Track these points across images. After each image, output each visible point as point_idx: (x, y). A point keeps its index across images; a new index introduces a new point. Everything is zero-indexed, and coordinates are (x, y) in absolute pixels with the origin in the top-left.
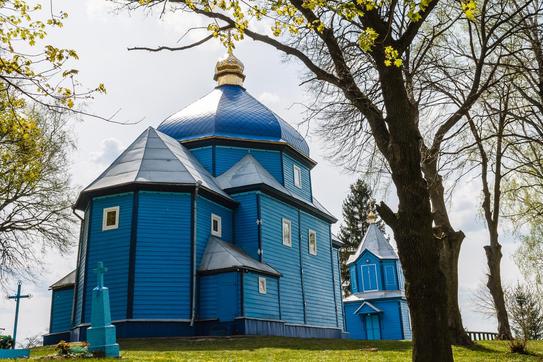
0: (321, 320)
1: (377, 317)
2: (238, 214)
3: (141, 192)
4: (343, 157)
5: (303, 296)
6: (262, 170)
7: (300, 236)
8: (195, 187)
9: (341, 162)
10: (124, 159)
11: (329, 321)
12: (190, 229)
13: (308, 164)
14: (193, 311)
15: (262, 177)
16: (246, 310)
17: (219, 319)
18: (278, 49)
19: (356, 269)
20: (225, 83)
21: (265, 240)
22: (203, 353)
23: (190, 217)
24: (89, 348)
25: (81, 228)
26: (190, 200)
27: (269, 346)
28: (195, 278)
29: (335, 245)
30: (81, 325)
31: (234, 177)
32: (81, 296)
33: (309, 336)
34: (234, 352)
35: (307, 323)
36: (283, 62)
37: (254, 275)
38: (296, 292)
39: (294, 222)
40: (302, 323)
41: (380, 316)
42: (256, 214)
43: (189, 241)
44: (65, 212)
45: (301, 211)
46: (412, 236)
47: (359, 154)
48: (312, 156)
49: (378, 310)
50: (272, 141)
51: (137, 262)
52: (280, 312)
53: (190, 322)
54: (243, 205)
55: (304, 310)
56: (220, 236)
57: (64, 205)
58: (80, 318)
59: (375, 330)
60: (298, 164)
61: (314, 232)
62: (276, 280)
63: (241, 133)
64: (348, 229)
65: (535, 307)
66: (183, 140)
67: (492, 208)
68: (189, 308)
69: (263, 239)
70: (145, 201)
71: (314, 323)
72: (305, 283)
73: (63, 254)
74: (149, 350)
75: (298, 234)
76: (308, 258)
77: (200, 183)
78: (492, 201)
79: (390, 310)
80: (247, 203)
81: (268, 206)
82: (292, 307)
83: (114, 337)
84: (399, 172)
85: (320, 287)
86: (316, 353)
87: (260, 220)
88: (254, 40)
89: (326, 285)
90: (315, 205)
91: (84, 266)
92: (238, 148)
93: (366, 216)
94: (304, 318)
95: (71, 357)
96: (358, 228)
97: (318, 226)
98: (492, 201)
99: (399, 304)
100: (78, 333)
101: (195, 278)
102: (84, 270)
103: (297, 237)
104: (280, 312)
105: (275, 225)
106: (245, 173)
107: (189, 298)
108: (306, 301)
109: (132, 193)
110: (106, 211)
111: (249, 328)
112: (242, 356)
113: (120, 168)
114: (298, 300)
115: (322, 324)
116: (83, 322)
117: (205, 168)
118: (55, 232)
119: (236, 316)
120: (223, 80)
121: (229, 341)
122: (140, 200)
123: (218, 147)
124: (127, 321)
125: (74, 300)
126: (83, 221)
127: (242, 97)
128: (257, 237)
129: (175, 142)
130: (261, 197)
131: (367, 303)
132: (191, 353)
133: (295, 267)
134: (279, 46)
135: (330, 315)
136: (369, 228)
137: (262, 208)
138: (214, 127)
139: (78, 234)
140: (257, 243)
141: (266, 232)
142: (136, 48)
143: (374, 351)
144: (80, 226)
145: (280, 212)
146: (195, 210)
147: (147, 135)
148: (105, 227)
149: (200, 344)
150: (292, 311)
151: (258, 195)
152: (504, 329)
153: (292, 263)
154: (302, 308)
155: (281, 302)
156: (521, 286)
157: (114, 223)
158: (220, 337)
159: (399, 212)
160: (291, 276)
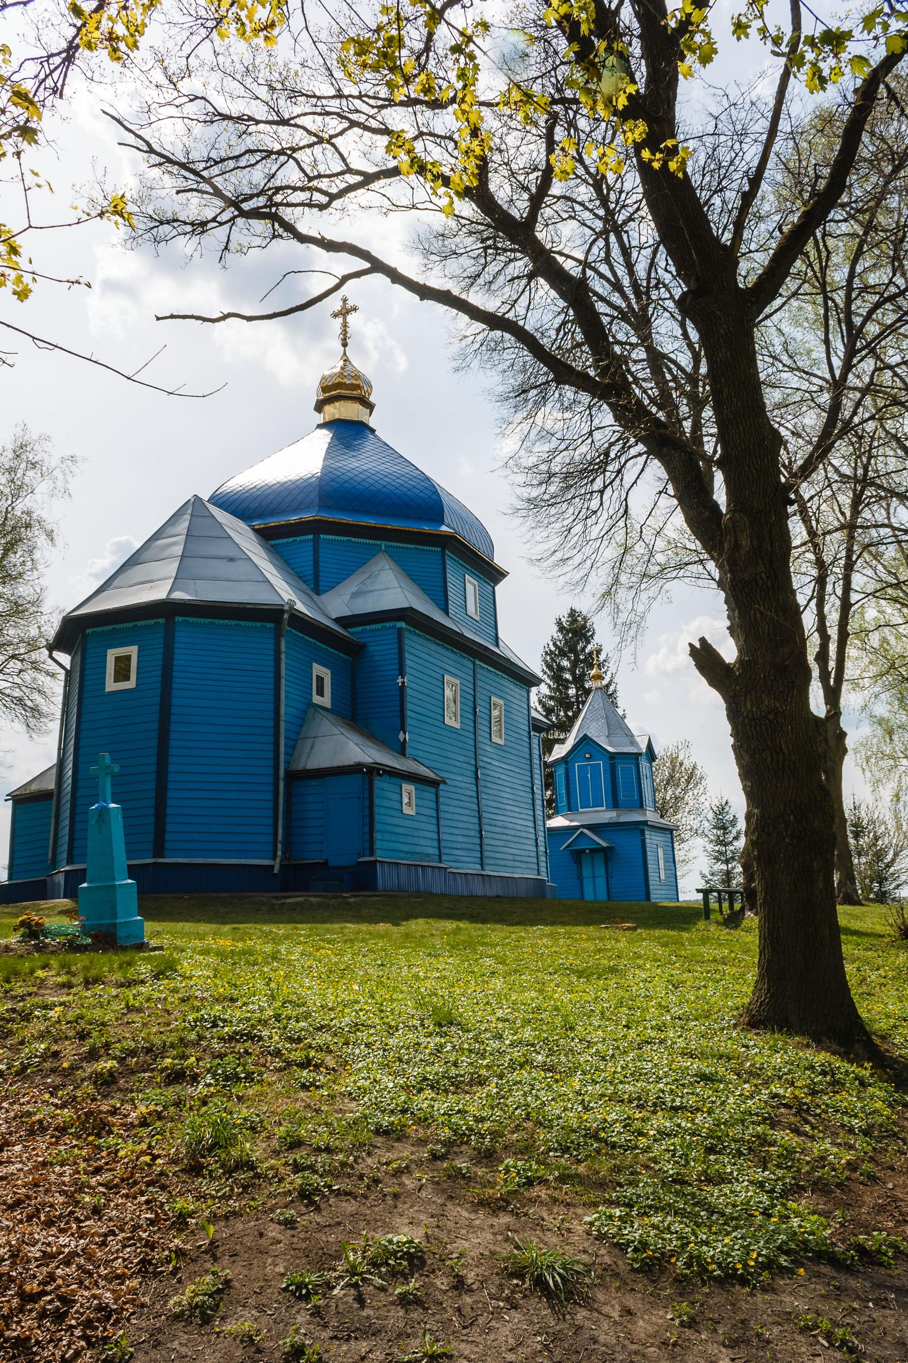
0: (511, 863)
1: (601, 856)
2: (364, 668)
3: (178, 619)
4: (564, 561)
5: (480, 818)
6: (407, 584)
7: (475, 708)
8: (282, 611)
9: (558, 571)
10: (149, 554)
11: (523, 865)
12: (272, 692)
13: (492, 574)
14: (279, 846)
15: (409, 595)
16: (378, 844)
17: (327, 861)
18: (471, 318)
19: (567, 770)
20: (337, 416)
21: (413, 715)
22: (303, 929)
23: (272, 669)
24: (83, 926)
25: (65, 687)
26: (273, 636)
27: (427, 915)
28: (282, 784)
29: (536, 726)
30: (67, 868)
31: (355, 595)
32: (66, 813)
33: (489, 894)
34: (364, 927)
35: (487, 867)
36: (457, 370)
37: (394, 780)
38: (468, 812)
39: (466, 683)
40: (475, 869)
41: (607, 854)
42: (397, 667)
43: (271, 715)
44: (34, 656)
45: (478, 662)
46: (769, 713)
47: (594, 556)
48: (499, 560)
49: (604, 844)
50: (426, 528)
51: (172, 752)
52: (439, 848)
53: (273, 867)
54: (371, 649)
55: (481, 845)
56: (329, 706)
57: (32, 646)
58: (65, 855)
59: (597, 880)
60: (473, 574)
61: (502, 702)
62: (433, 790)
63: (369, 513)
64: (551, 698)
65: (880, 842)
66: (257, 523)
67: (832, 664)
68: (270, 838)
69: (409, 713)
70: (186, 634)
71: (498, 868)
72: (484, 796)
73: (34, 735)
74: (199, 921)
75: (472, 704)
76: (488, 749)
77: (291, 604)
78: (833, 648)
79: (626, 844)
80: (379, 645)
81: (420, 652)
82: (460, 839)
83: (134, 904)
84: (746, 574)
85: (510, 802)
86: (519, 932)
87: (403, 677)
88: (422, 299)
89: (519, 799)
90: (502, 651)
91: (71, 757)
92: (363, 540)
93: (583, 674)
94: (481, 858)
95: (46, 946)
96: (568, 696)
97: (508, 691)
98: (833, 648)
99: (643, 833)
100: (62, 882)
101: (282, 784)
102: (71, 765)
103: (471, 710)
104: (439, 848)
105: (432, 687)
106: (376, 587)
107: (271, 821)
108: (485, 827)
109: (162, 621)
110: (112, 654)
111: (383, 878)
112: (381, 937)
113: (138, 573)
114: (471, 826)
115: (511, 870)
116: (70, 861)
117: (300, 577)
118: (17, 693)
119: (360, 855)
120: (333, 411)
121: (348, 904)
122: (177, 633)
123: (325, 537)
124: (155, 863)
125: (53, 821)
126: (68, 673)
127: (369, 444)
128: (398, 708)
129: (241, 525)
130: (406, 634)
131: (585, 831)
132: (280, 930)
133: (465, 766)
134: (475, 313)
135: (527, 853)
136: (591, 696)
137: (407, 655)
138: (317, 501)
139: (59, 699)
140: (398, 721)
141: (414, 700)
142: (172, 317)
143: (629, 929)
144: (62, 684)
145: (439, 663)
146: (283, 656)
147: (190, 511)
148: (111, 686)
149: (293, 908)
150: (459, 846)
151: (400, 631)
152: (846, 884)
153: (461, 758)
154: (478, 841)
155: (442, 829)
156: (857, 804)
157: (127, 678)
158: (331, 894)
159: (740, 660)
160: (459, 781)
